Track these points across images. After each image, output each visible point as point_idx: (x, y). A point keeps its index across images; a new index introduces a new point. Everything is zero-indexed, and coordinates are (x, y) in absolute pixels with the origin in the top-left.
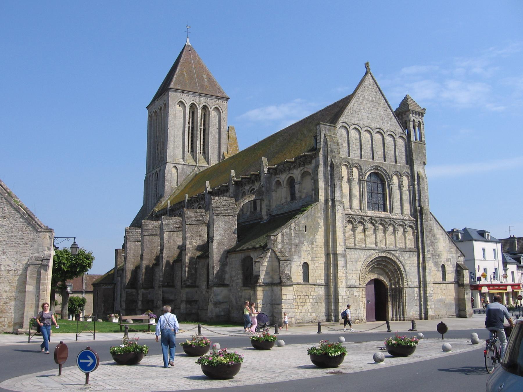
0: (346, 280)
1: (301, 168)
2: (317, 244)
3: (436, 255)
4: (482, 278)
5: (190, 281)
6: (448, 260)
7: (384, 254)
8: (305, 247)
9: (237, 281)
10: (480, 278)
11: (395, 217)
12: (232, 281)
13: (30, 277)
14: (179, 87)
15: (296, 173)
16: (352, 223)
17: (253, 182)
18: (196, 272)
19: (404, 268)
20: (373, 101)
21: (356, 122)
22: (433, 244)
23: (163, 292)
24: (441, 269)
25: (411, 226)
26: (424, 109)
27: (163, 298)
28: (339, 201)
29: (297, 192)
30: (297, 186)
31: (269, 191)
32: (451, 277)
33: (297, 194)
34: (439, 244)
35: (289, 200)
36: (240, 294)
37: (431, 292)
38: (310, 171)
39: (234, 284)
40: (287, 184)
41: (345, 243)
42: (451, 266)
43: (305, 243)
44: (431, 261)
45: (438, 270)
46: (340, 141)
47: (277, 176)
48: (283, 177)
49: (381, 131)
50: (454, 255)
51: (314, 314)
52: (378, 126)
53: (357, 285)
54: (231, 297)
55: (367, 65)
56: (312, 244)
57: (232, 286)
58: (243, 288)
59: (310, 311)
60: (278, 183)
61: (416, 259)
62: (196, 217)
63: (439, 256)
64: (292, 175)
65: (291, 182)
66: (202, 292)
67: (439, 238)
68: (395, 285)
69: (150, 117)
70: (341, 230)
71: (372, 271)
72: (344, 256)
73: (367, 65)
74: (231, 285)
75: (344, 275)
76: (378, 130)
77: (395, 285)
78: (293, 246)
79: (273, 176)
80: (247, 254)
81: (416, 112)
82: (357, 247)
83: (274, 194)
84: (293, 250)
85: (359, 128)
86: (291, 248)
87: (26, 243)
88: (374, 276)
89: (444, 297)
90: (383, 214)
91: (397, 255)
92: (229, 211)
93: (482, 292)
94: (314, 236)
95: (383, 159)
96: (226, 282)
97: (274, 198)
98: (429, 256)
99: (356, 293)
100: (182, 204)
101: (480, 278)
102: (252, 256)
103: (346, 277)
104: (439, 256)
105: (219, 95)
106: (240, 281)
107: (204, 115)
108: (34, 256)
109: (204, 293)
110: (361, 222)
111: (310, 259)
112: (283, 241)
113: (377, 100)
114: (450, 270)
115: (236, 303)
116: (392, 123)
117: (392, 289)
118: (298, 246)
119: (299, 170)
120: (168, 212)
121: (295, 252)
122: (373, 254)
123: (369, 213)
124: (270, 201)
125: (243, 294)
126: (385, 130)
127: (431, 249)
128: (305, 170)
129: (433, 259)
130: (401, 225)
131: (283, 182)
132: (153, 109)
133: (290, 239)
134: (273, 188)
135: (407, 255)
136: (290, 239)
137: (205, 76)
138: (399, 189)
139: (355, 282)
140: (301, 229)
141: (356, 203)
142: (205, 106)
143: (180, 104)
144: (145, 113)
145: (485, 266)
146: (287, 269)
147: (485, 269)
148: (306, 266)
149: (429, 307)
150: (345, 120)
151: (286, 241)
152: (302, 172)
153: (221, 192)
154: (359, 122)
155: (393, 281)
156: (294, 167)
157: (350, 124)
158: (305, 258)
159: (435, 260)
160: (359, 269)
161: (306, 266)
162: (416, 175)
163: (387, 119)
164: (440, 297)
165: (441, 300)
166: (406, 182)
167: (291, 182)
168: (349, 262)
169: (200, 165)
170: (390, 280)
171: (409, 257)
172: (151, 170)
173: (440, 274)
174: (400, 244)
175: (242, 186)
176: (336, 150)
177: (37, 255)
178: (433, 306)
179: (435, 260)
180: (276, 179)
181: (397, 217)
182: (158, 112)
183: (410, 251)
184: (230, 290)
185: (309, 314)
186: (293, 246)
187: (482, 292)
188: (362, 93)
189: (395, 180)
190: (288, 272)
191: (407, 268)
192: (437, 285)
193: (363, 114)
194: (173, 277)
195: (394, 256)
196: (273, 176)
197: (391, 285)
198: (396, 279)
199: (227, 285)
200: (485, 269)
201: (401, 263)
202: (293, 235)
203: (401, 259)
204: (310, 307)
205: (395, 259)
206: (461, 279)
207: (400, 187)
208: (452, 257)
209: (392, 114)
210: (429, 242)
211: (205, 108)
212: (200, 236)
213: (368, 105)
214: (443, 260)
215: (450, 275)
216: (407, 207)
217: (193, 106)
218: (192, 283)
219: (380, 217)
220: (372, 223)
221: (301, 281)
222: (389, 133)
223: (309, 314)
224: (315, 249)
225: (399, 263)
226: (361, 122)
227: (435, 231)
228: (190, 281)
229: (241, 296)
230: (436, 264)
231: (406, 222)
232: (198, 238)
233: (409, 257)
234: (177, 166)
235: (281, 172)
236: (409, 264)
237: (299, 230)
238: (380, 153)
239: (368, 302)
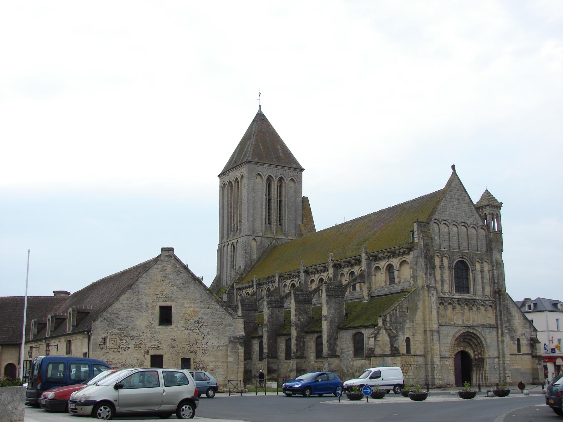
0: (440, 351)
1: (400, 257)
2: (417, 322)
3: (512, 330)
4: (556, 350)
5: (299, 353)
6: (523, 334)
7: (469, 330)
8: (408, 325)
9: (348, 353)
10: (554, 349)
11: (477, 298)
12: (343, 353)
13: (231, 352)
14: (256, 160)
15: (395, 262)
16: (443, 304)
17: (352, 265)
18: (304, 344)
19: (486, 342)
20: (458, 199)
21: (445, 218)
22: (509, 321)
23: (268, 363)
24: (516, 342)
25: (491, 306)
26: (501, 203)
27: (268, 368)
28: (433, 287)
29: (396, 277)
30: (396, 273)
31: (369, 274)
32: (525, 349)
33: (396, 280)
34: (514, 321)
35: (388, 283)
36: (351, 363)
37: (508, 362)
38: (408, 261)
39: (345, 356)
40: (386, 270)
41: (438, 321)
42: (525, 340)
43: (408, 322)
44: (508, 336)
45: (514, 344)
46: (433, 236)
47: (377, 262)
48: (383, 264)
49: (466, 225)
50: (528, 330)
51: (415, 380)
52: (463, 221)
53: (447, 355)
54: (342, 366)
55: (453, 167)
56: (413, 322)
57: (343, 357)
58: (354, 359)
59: (412, 377)
60: (378, 268)
61: (495, 333)
62: (303, 296)
63: (514, 331)
64: (391, 263)
65: (390, 268)
66: (310, 362)
67: (515, 316)
68: (478, 356)
69: (223, 187)
70: (435, 311)
71: (459, 345)
72: (438, 332)
73: (453, 167)
74: (341, 356)
75: (438, 347)
76: (463, 224)
77: (478, 356)
78: (398, 325)
79: (373, 262)
80: (357, 331)
81: (494, 206)
82: (447, 324)
83: (373, 277)
84: (399, 327)
85: (448, 223)
86: (397, 326)
87: (225, 327)
88: (460, 349)
89: (519, 367)
90: (466, 296)
91: (479, 330)
92: (339, 294)
93: (557, 364)
94: (414, 316)
95: (467, 248)
96: (338, 354)
97: (374, 281)
98: (507, 331)
99: (447, 363)
100: (272, 279)
101: (554, 349)
102: (363, 332)
103: (440, 349)
104: (514, 331)
105: (294, 166)
106: (351, 352)
107: (280, 186)
108: (232, 336)
109: (312, 363)
110: (450, 303)
111: (411, 334)
112: (391, 321)
113: (462, 197)
114: (524, 342)
115: (348, 371)
116: (474, 217)
117: (476, 359)
118: (402, 324)
119: (398, 259)
120: (255, 286)
121: (400, 329)
122: (460, 330)
123: (457, 296)
124: (370, 284)
125: (355, 363)
126: (469, 223)
127: (507, 325)
128: (404, 259)
129: (509, 333)
130: (482, 305)
131: (383, 268)
132: (227, 179)
133: (396, 319)
134: (373, 273)
135: (487, 330)
136: (396, 319)
137: (279, 147)
138: (479, 273)
139: (447, 353)
140: (404, 310)
141: (446, 288)
142: (281, 178)
143: (258, 176)
144: (217, 182)
145: (559, 337)
146: (396, 343)
147: (559, 341)
148: (408, 340)
149: (507, 375)
150: (437, 218)
151: (393, 320)
152: (401, 261)
153: (318, 272)
154: (447, 218)
155: (476, 353)
156: (393, 257)
157: (440, 220)
158: (408, 334)
159: (512, 335)
160: (450, 342)
161: (408, 340)
162: (494, 261)
163: (470, 214)
164: (516, 367)
165: (517, 370)
166: (486, 267)
167: (390, 268)
168: (442, 337)
169: (278, 237)
170: (474, 352)
171: (490, 332)
172: (225, 240)
173: (515, 347)
174: (481, 322)
175: (340, 268)
176: (430, 244)
177: (234, 335)
178: (510, 375)
179: (512, 335)
180: (376, 265)
181: (480, 298)
182: (233, 183)
183: (491, 326)
184: (341, 360)
185: (411, 380)
186: (398, 325)
187: (557, 364)
188: (450, 193)
189: (478, 266)
190: (397, 346)
191: (488, 341)
192: (514, 357)
193: (451, 211)
194: (276, 349)
195: (478, 331)
196: (373, 262)
197: (475, 355)
198: (479, 351)
199: (338, 357)
200: (559, 341)
201: (483, 337)
202: (398, 315)
203: (483, 334)
204: (411, 374)
205: (478, 334)
206: (535, 351)
207: (482, 271)
208: (526, 332)
209: (474, 209)
210: (506, 319)
211: (281, 180)
212: (307, 313)
213: (455, 203)
214: (518, 334)
215: (525, 348)
216: (488, 290)
217: (269, 178)
218: (301, 355)
219: (465, 299)
220: (459, 304)
221: (405, 352)
222: (472, 226)
223: (411, 380)
224: (415, 326)
225: (481, 337)
226: (449, 218)
227: (511, 309)
228: (299, 353)
229: (353, 366)
230: (512, 338)
231: (487, 303)
232: (304, 315)
233: (490, 332)
234: (256, 238)
235: (381, 259)
236: (489, 338)
237: (402, 311)
238: (464, 244)
239: (456, 369)
